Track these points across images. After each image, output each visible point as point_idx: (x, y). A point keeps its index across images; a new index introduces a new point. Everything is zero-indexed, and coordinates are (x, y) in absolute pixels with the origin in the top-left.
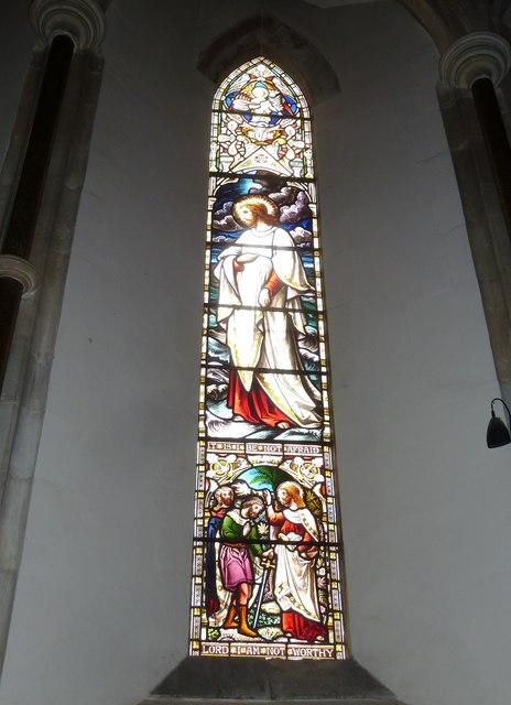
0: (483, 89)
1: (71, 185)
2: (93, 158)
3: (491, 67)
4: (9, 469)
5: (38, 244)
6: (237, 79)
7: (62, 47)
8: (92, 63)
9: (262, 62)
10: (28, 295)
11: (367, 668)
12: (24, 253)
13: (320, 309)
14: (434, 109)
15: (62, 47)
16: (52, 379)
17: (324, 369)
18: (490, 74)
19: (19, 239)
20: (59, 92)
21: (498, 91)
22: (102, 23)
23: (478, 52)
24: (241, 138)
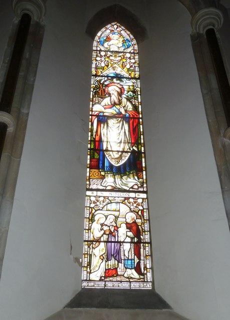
0: (211, 33)
1: (24, 111)
2: (37, 84)
3: (215, 22)
4: (17, 125)
5: (15, 105)
6: (102, 33)
7: (26, 19)
8: (39, 27)
9: (115, 24)
10: (10, 130)
11: (166, 300)
12: (8, 111)
13: (143, 151)
14: (189, 38)
15: (26, 19)
16: (28, 126)
17: (141, 116)
18: (214, 26)
19: (4, 105)
20: (25, 37)
21: (218, 36)
22: (44, 11)
23: (210, 17)
24: (107, 59)
